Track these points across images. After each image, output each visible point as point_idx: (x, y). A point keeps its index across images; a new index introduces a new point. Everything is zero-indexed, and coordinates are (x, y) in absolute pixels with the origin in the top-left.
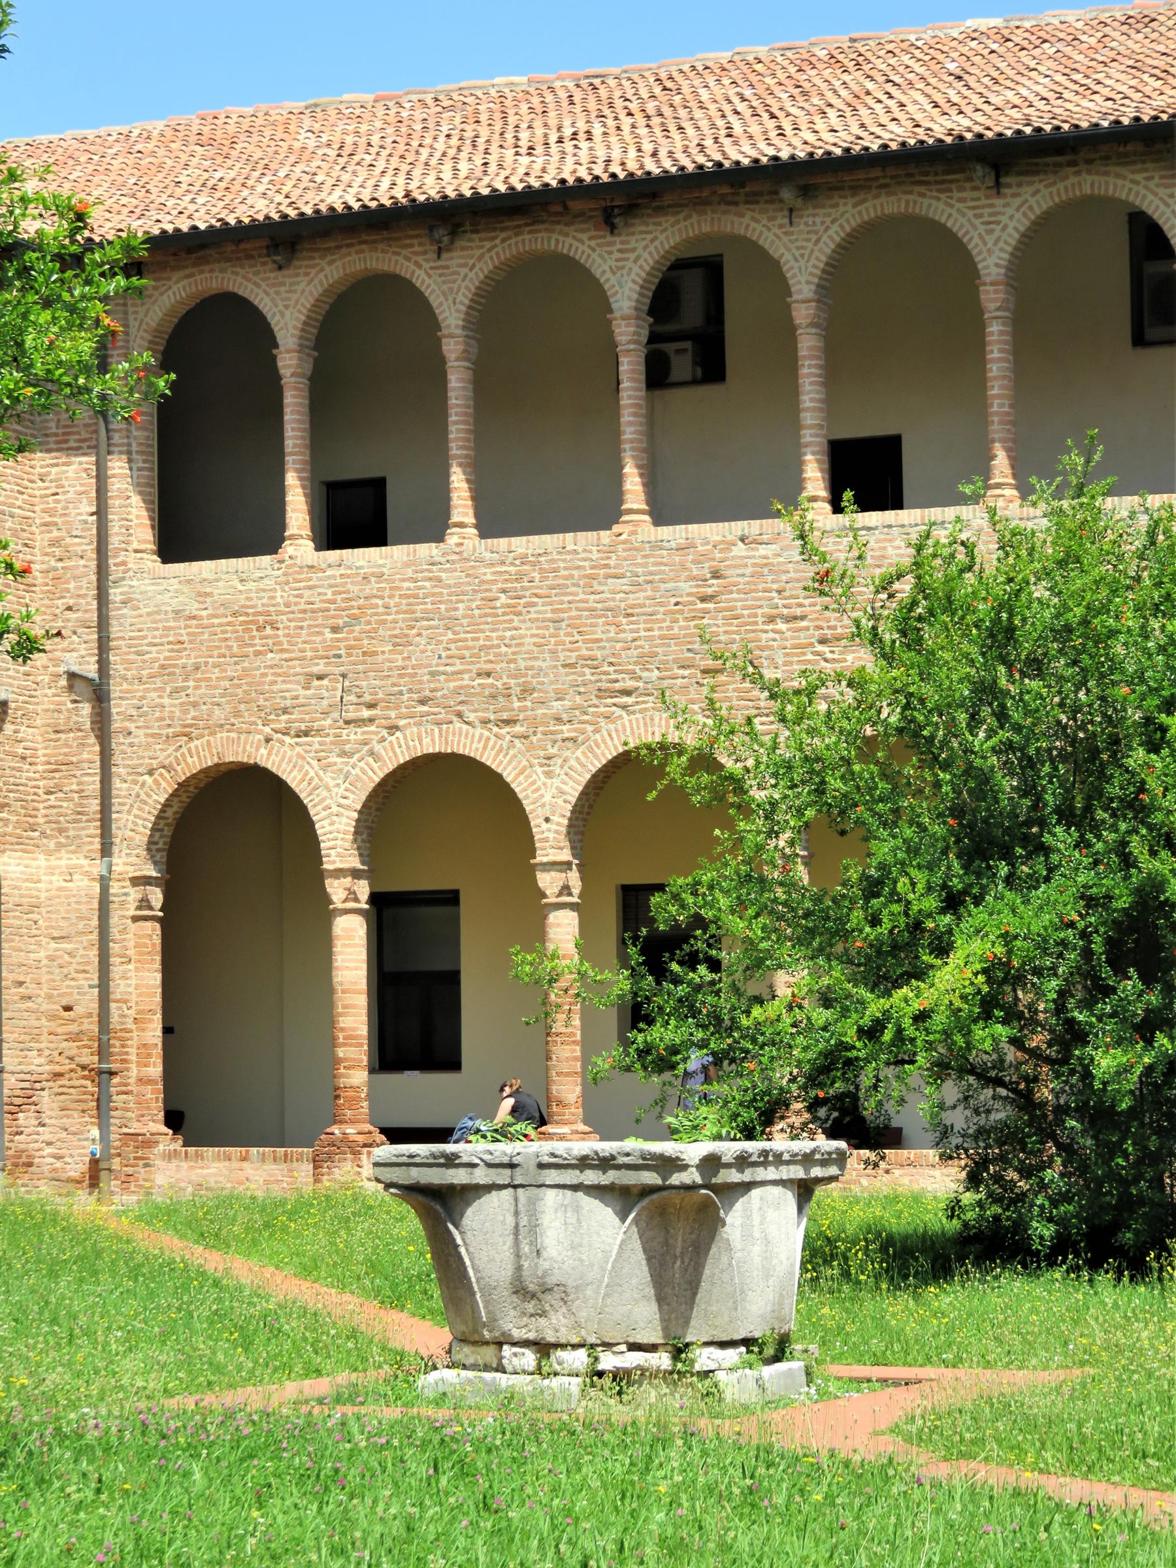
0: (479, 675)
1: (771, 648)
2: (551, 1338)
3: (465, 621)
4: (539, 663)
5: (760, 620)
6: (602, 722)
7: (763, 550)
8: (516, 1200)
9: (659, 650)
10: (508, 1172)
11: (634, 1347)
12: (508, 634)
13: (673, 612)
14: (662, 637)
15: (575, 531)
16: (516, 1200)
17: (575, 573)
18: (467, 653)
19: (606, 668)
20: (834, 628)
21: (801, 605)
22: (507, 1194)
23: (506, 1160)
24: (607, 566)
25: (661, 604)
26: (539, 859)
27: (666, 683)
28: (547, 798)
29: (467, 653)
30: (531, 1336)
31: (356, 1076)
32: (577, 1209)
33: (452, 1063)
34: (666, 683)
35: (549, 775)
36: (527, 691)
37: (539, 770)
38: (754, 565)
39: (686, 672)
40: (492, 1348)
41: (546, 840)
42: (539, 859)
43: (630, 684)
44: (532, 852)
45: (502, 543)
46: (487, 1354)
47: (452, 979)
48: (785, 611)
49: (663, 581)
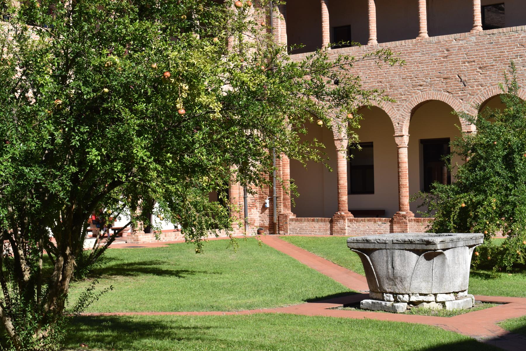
0: (378, 82)
1: (464, 71)
2: (397, 292)
3: (373, 67)
4: (395, 78)
5: (460, 63)
6: (413, 94)
7: (461, 42)
8: (387, 253)
9: (431, 73)
10: (384, 245)
11: (421, 294)
12: (386, 70)
13: (434, 62)
14: (431, 69)
15: (405, 39)
16: (387, 253)
17: (405, 52)
18: (374, 76)
19: (415, 79)
20: (483, 64)
21: (473, 58)
22: (384, 251)
23: (384, 242)
24: (415, 49)
25: (431, 59)
26: (396, 135)
27: (432, 82)
28: (398, 117)
29: (374, 76)
30: (392, 291)
31: (344, 198)
32: (404, 256)
33: (372, 192)
34: (432, 82)
35: (399, 110)
36: (391, 86)
37: (395, 109)
38: (459, 47)
39: (438, 79)
40: (381, 294)
41: (398, 129)
42: (396, 135)
43: (422, 83)
44: (394, 133)
45: (384, 44)
46: (379, 296)
47: (372, 167)
48: (468, 60)
49: (431, 53)
